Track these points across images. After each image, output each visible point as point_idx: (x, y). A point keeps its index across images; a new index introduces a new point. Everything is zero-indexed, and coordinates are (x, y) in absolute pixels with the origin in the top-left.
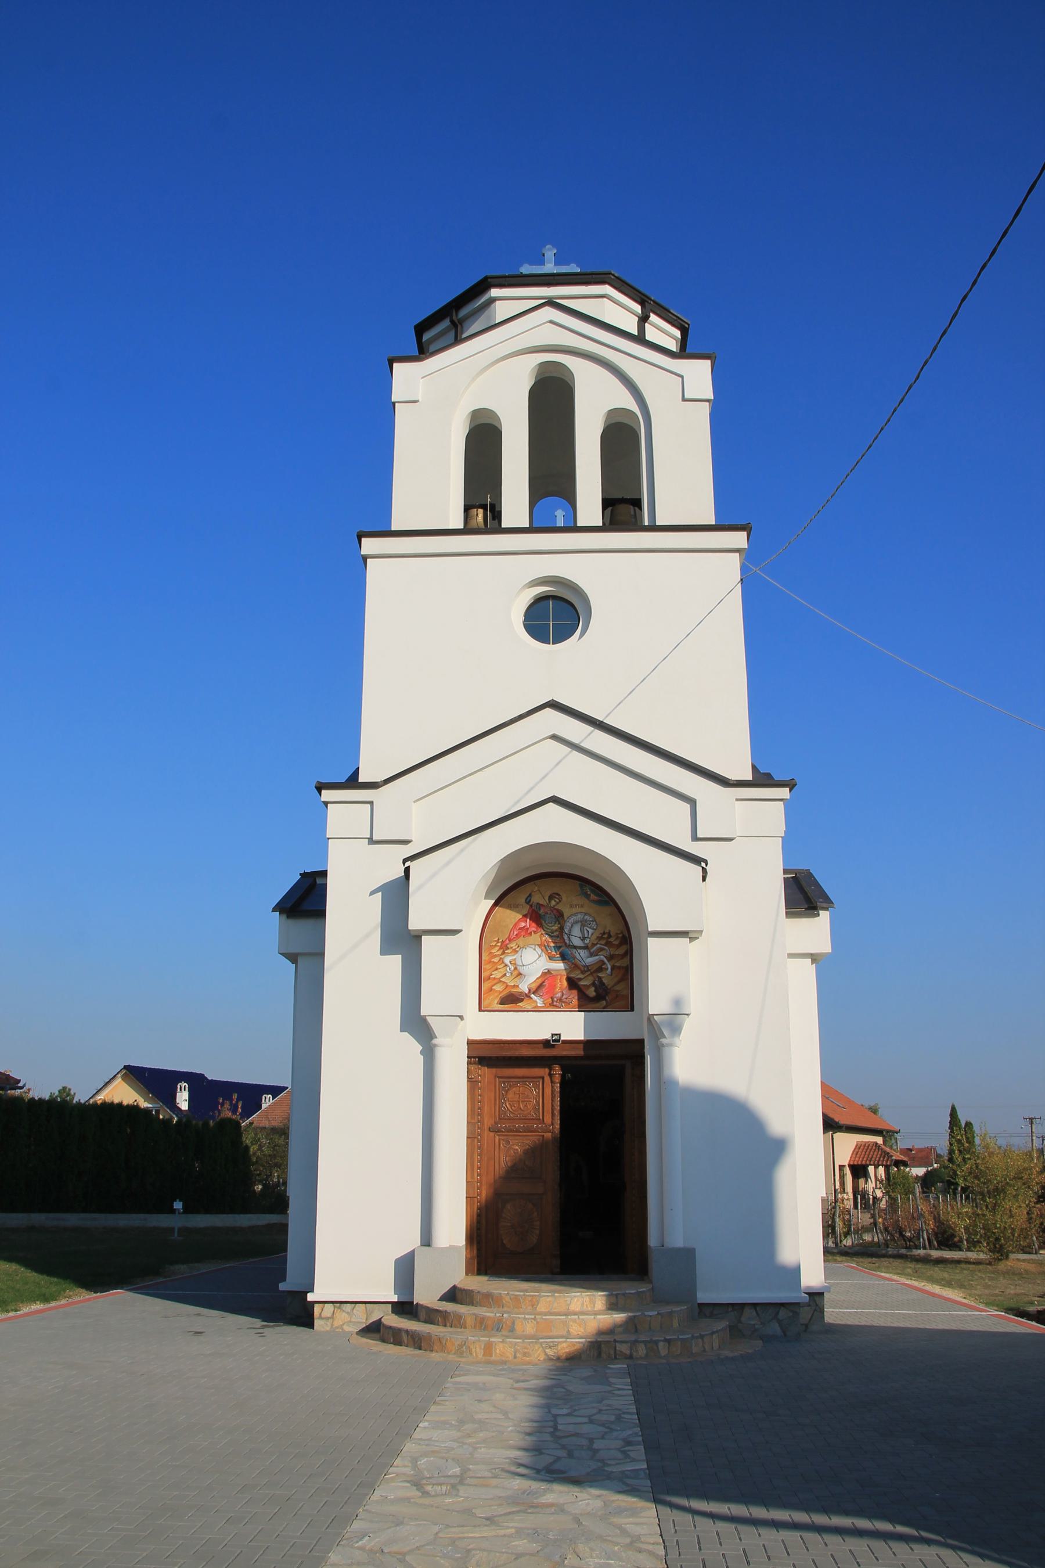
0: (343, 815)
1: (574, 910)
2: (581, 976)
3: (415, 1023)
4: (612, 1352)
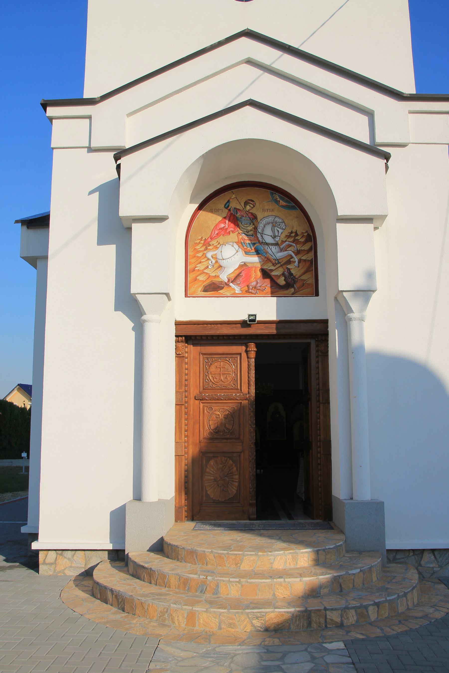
0: (66, 127)
1: (266, 214)
2: (273, 268)
3: (129, 304)
4: (322, 620)
